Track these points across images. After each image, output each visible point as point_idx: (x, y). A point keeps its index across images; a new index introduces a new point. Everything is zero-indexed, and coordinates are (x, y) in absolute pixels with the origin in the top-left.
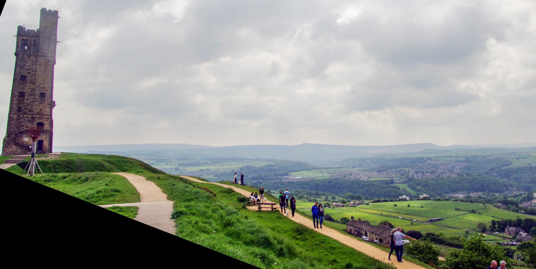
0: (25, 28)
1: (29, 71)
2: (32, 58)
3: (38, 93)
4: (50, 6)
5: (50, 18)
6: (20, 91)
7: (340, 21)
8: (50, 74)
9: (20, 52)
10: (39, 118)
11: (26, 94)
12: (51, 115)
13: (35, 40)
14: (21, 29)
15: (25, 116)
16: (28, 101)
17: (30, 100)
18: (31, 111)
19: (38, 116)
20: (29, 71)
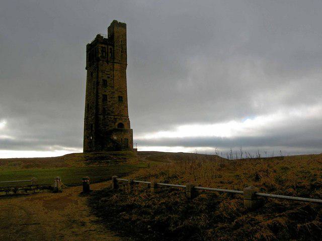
2: (110, 64)
3: (116, 96)
5: (117, 30)
15: (109, 116)
18: (112, 112)
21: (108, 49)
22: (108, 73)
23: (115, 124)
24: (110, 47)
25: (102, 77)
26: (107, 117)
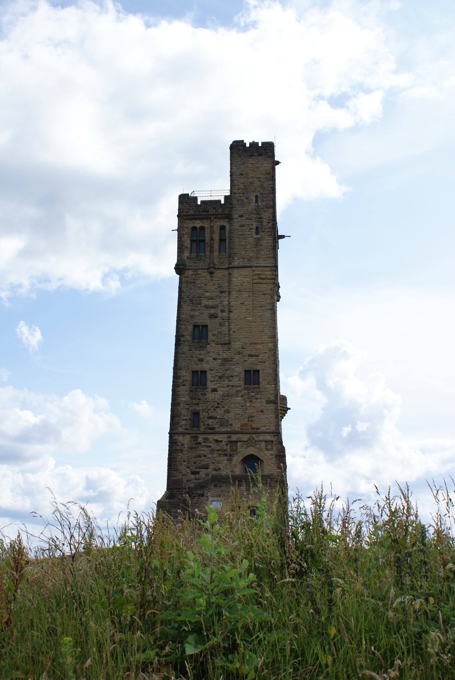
0: (196, 198)
1: (212, 311)
2: (218, 274)
3: (239, 370)
4: (252, 136)
5: (254, 163)
6: (195, 368)
7: (22, 323)
8: (268, 314)
9: (188, 263)
10: (248, 443)
11: (209, 376)
12: (278, 434)
13: (223, 228)
14: (186, 201)
15: (211, 437)
16: (216, 396)
17: (220, 392)
18: (224, 422)
19: (245, 437)
20: (212, 311)
21: (212, 232)
22: (211, 303)
23: (230, 460)
24: (218, 224)
25: (192, 317)
26: (206, 440)
